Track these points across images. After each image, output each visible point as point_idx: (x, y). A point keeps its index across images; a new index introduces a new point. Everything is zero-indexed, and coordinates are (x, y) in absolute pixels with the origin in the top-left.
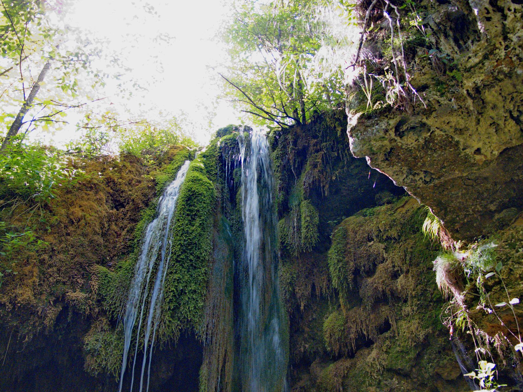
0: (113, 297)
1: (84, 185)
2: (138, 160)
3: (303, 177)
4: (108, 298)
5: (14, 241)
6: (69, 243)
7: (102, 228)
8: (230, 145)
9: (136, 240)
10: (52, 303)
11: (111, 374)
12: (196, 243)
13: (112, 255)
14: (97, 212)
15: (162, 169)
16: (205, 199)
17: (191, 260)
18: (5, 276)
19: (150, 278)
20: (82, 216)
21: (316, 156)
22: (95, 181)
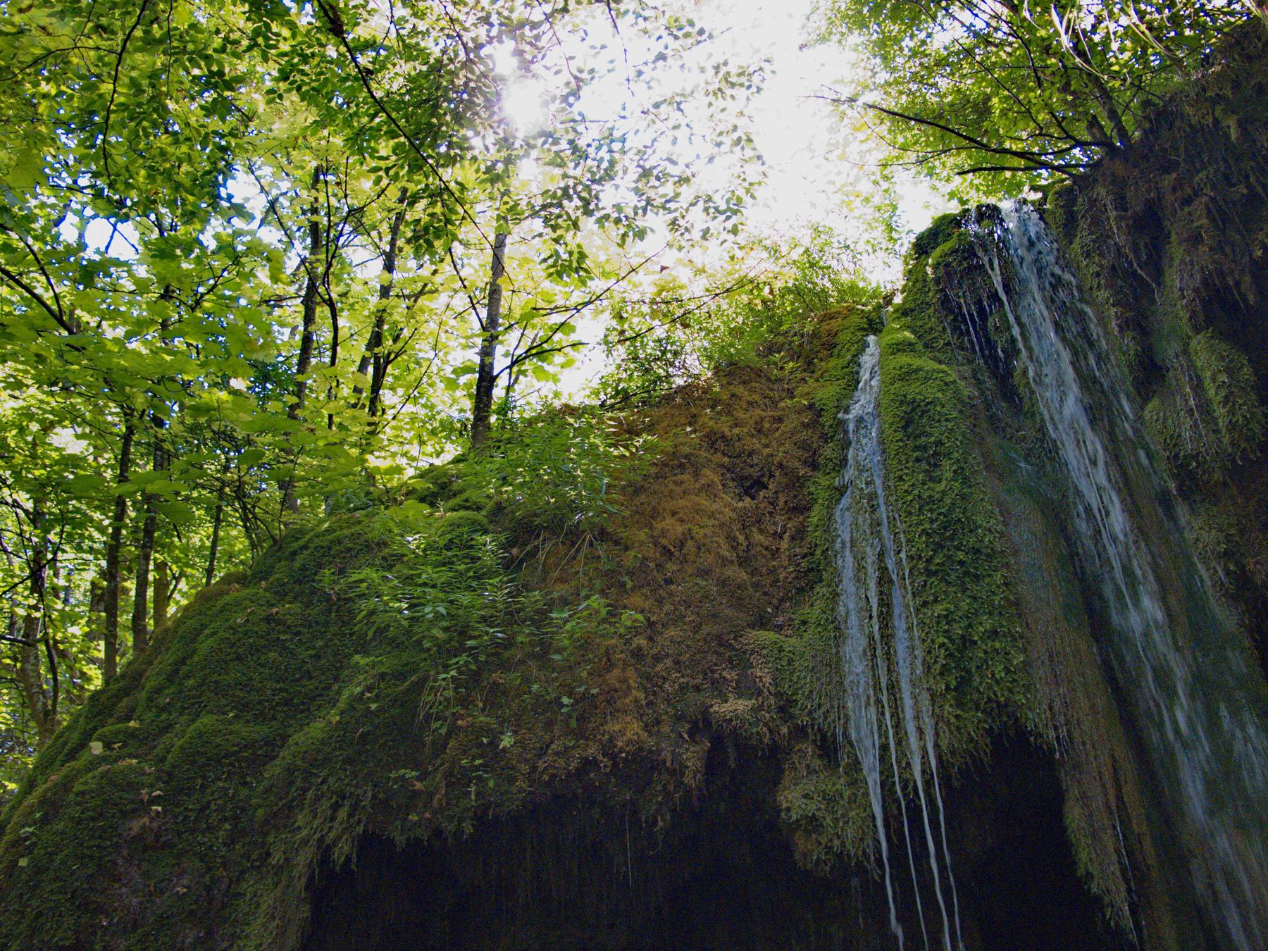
0: (811, 692)
2: (759, 373)
3: (1173, 279)
5: (568, 626)
6: (677, 599)
9: (818, 552)
10: (686, 736)
11: (859, 864)
12: (959, 520)
13: (775, 601)
14: (711, 516)
15: (815, 376)
16: (944, 410)
17: (961, 563)
18: (577, 702)
19: (880, 628)
20: (684, 534)
21: (1190, 214)
22: (686, 450)
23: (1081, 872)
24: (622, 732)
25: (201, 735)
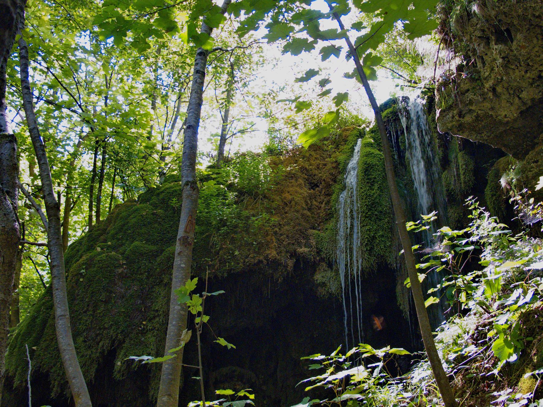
1: (286, 176)
4: (323, 250)
7: (307, 205)
8: (392, 118)
15: (339, 150)
17: (376, 215)
23: (398, 304)
24: (270, 254)
25: (136, 247)
